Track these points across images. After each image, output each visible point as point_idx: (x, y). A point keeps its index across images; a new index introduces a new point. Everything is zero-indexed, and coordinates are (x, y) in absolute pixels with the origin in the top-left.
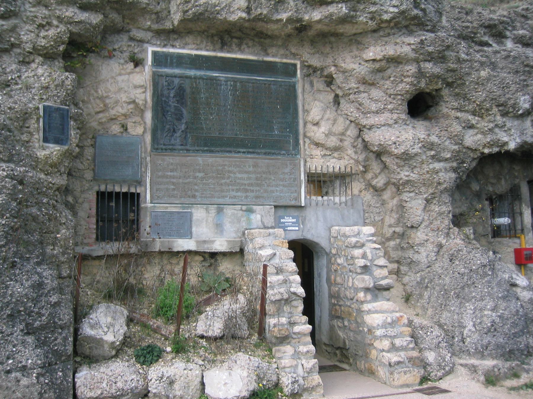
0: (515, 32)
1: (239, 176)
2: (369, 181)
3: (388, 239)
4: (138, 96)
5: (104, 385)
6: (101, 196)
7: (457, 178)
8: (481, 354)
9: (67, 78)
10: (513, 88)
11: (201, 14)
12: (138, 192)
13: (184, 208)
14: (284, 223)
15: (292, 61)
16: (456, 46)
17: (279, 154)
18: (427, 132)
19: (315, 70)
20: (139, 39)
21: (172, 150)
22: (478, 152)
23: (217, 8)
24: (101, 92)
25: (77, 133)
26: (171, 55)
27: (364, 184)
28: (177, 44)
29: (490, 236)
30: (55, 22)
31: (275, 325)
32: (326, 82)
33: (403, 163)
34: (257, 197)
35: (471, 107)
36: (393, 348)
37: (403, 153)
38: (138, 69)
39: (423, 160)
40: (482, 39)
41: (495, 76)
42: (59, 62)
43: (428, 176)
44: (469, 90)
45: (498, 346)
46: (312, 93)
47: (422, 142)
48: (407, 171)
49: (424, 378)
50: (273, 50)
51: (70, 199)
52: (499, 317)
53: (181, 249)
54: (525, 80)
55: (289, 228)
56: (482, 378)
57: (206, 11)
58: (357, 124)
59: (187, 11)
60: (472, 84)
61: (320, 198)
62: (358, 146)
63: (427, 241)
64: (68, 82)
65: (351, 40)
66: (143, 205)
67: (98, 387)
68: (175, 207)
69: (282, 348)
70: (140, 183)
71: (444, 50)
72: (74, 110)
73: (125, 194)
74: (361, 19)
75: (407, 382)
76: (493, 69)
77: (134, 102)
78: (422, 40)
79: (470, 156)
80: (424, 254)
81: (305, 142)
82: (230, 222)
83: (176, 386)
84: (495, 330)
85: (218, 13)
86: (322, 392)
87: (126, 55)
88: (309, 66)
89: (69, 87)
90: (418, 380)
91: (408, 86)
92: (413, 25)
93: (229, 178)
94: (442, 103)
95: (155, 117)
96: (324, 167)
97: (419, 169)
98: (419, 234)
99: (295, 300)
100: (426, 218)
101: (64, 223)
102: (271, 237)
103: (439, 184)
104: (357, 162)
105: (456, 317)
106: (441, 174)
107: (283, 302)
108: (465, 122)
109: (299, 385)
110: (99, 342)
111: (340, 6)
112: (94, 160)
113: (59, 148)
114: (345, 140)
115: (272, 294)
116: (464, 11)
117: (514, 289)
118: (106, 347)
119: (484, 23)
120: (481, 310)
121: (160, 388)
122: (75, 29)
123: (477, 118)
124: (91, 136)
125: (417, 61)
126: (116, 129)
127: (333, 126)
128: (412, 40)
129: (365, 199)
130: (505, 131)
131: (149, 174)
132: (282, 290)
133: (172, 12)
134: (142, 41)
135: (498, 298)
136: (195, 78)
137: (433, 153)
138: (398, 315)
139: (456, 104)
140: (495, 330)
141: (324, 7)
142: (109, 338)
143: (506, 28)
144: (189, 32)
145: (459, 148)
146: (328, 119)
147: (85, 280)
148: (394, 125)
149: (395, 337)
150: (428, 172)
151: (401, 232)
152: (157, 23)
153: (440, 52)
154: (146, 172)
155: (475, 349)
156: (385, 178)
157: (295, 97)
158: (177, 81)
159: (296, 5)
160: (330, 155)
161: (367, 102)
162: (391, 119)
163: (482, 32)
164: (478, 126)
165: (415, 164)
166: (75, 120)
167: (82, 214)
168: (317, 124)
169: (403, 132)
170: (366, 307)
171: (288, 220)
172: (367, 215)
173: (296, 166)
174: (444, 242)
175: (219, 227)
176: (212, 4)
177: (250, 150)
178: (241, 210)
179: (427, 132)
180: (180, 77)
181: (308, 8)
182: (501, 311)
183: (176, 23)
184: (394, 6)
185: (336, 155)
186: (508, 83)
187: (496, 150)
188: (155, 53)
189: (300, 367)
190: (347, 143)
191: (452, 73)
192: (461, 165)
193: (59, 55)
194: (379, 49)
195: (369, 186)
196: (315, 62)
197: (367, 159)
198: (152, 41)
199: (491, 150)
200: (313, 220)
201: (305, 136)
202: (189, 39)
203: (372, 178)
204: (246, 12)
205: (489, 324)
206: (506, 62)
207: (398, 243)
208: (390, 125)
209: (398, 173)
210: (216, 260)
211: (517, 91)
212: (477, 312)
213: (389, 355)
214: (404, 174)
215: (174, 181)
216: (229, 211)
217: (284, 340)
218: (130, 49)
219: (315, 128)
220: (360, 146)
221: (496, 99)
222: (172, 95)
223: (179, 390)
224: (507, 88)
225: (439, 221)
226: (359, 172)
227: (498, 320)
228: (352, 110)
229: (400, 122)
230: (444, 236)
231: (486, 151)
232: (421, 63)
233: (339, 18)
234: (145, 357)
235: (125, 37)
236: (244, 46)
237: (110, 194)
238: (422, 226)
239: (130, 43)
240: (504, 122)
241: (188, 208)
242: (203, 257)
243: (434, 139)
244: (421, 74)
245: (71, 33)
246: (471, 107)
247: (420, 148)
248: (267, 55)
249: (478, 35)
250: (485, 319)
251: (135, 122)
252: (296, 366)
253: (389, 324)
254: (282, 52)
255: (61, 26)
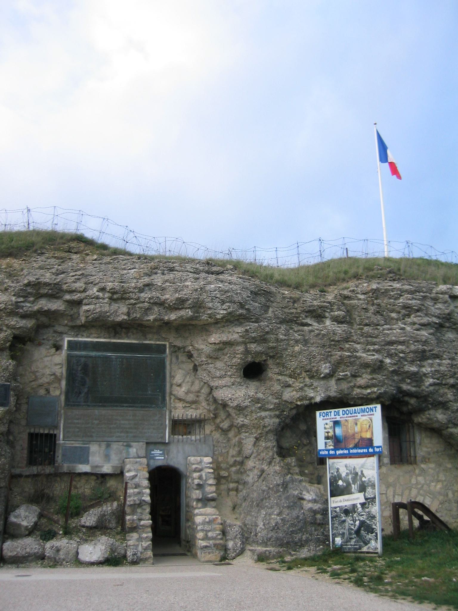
0: (332, 313)
1: (122, 422)
2: (218, 424)
3: (231, 466)
4: (57, 370)
5: (19, 549)
6: (32, 436)
7: (280, 423)
8: (265, 543)
9: (10, 364)
10: (318, 358)
11: (97, 318)
12: (55, 433)
13: (84, 444)
14: (154, 454)
15: (163, 343)
16: (276, 330)
17: (151, 407)
18: (256, 391)
19: (179, 348)
20: (60, 332)
21: (78, 405)
22: (293, 404)
23: (108, 314)
24: (34, 368)
25: (15, 399)
26: (80, 343)
27: (214, 426)
28: (85, 334)
29: (316, 464)
30: (5, 328)
31: (129, 520)
32: (187, 355)
33: (238, 413)
34: (134, 437)
35: (288, 372)
36: (206, 538)
37: (237, 406)
38: (58, 352)
39: (252, 410)
40: (303, 321)
41: (305, 350)
42: (6, 352)
43: (256, 421)
44: (286, 361)
45: (277, 539)
46: (177, 364)
47: (251, 398)
48: (242, 418)
49: (224, 557)
50: (150, 336)
51: (11, 438)
52: (282, 520)
53: (80, 471)
54: (330, 352)
55: (157, 458)
56: (256, 557)
57: (101, 316)
58: (209, 385)
59: (88, 317)
60: (288, 356)
61: (180, 437)
62: (210, 400)
63: (254, 467)
64: (11, 367)
65: (202, 328)
66: (57, 442)
67: (15, 551)
68: (79, 443)
69: (131, 534)
70: (57, 427)
71: (264, 335)
72: (14, 384)
73: (47, 435)
74: (203, 317)
75: (211, 559)
76: (304, 345)
77: (54, 374)
78: (246, 330)
79: (288, 407)
80: (251, 477)
81: (170, 398)
82: (115, 454)
83: (61, 553)
84: (278, 528)
85: (108, 317)
86: (152, 561)
87: (51, 342)
88: (175, 346)
89: (11, 370)
90: (219, 559)
91: (239, 360)
92: (241, 319)
93: (115, 424)
94: (269, 370)
95: (68, 384)
96: (185, 415)
97: (250, 417)
98: (250, 462)
99: (144, 505)
100: (255, 451)
101: (4, 455)
102: (137, 464)
103: (264, 426)
104: (209, 411)
105: (254, 519)
106: (266, 420)
107: (137, 506)
108: (283, 383)
109: (137, 557)
110: (19, 526)
111: (187, 310)
112: (27, 413)
113: (3, 409)
114: (201, 396)
115: (130, 501)
116: (292, 300)
117: (302, 501)
118: (23, 529)
119: (305, 310)
120: (270, 515)
121: (51, 553)
122: (17, 332)
123: (293, 380)
124: (26, 397)
125: (245, 343)
126: (42, 392)
127: (191, 386)
128: (240, 329)
129: (215, 437)
130: (313, 389)
131: (62, 422)
132: (136, 498)
133: (81, 315)
134: (61, 333)
135: (283, 507)
136: (96, 357)
137: (259, 405)
138: (214, 517)
139: (277, 370)
140: (278, 528)
141: (178, 311)
142: (25, 523)
143: (325, 311)
144: (93, 326)
145: (279, 401)
146: (188, 382)
147: (16, 490)
148: (231, 386)
149: (209, 531)
150: (256, 419)
151: (241, 461)
152: (71, 321)
153: (261, 336)
154: (60, 420)
155: (262, 541)
156: (229, 422)
157: (164, 367)
158: (83, 360)
159: (159, 310)
160: (189, 407)
161: (213, 370)
162: (230, 382)
163: (304, 316)
164: (294, 385)
165: (246, 413)
166: (14, 391)
167: (18, 448)
168: (180, 385)
169: (238, 391)
170: (196, 511)
171: (157, 452)
172: (216, 448)
173: (163, 416)
174: (266, 468)
175: (107, 457)
176: (104, 312)
177: (131, 405)
178: (123, 445)
179: (256, 391)
180: (85, 357)
181: (168, 312)
182: (284, 516)
183: (83, 322)
184: (224, 309)
185: (193, 406)
186: (315, 355)
187: (306, 402)
188: (69, 342)
189: (140, 546)
190: (202, 398)
191: (272, 350)
192: (282, 413)
193: (7, 348)
194: (218, 335)
195: (218, 428)
196: (178, 343)
197: (216, 409)
198: (69, 333)
199: (302, 403)
200: (175, 452)
201: (171, 394)
202: (93, 331)
203: (220, 422)
204: (127, 315)
205: (274, 524)
206: (316, 338)
207: (238, 468)
208: (229, 386)
209: (237, 419)
210: (105, 479)
211: (320, 360)
212: (267, 516)
213: (202, 542)
214: (240, 420)
215: (79, 426)
216: (115, 446)
217: (134, 529)
218: (54, 339)
219: (178, 388)
220: (211, 400)
221: (303, 367)
222: (79, 369)
223: (63, 555)
224: (313, 358)
225: (265, 453)
226: (210, 418)
227: (280, 522)
228: (205, 375)
229: (236, 384)
230: (267, 464)
231: (299, 403)
232: (248, 344)
233: (187, 318)
234: (45, 536)
235: (51, 330)
236: (130, 334)
237: (37, 434)
238: (252, 457)
239: (53, 335)
240: (311, 383)
241: (87, 444)
242: (97, 476)
243: (260, 395)
244: (247, 352)
245: (14, 334)
246: (288, 372)
247: (250, 402)
248: (146, 339)
249: (301, 318)
250: (272, 521)
251: (54, 388)
252: (138, 545)
253: (207, 522)
254: (156, 337)
255: (8, 330)
